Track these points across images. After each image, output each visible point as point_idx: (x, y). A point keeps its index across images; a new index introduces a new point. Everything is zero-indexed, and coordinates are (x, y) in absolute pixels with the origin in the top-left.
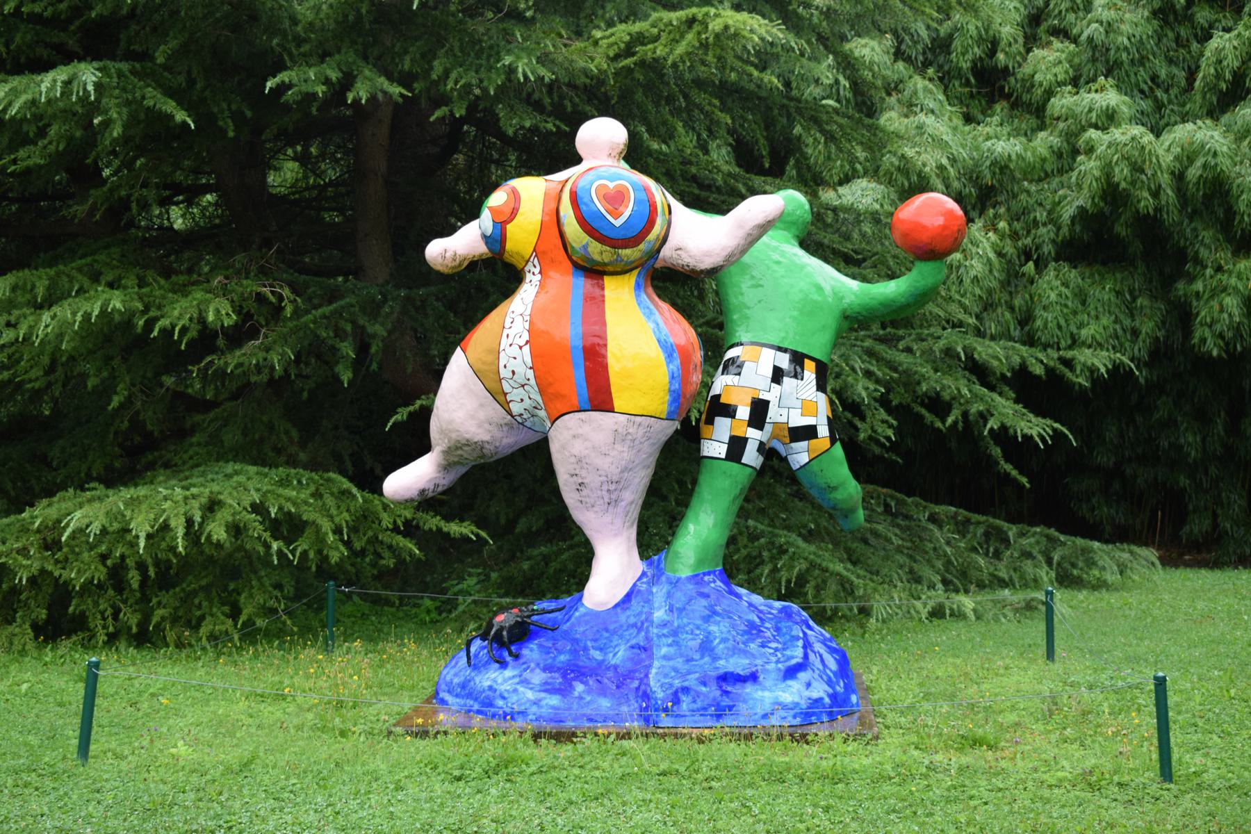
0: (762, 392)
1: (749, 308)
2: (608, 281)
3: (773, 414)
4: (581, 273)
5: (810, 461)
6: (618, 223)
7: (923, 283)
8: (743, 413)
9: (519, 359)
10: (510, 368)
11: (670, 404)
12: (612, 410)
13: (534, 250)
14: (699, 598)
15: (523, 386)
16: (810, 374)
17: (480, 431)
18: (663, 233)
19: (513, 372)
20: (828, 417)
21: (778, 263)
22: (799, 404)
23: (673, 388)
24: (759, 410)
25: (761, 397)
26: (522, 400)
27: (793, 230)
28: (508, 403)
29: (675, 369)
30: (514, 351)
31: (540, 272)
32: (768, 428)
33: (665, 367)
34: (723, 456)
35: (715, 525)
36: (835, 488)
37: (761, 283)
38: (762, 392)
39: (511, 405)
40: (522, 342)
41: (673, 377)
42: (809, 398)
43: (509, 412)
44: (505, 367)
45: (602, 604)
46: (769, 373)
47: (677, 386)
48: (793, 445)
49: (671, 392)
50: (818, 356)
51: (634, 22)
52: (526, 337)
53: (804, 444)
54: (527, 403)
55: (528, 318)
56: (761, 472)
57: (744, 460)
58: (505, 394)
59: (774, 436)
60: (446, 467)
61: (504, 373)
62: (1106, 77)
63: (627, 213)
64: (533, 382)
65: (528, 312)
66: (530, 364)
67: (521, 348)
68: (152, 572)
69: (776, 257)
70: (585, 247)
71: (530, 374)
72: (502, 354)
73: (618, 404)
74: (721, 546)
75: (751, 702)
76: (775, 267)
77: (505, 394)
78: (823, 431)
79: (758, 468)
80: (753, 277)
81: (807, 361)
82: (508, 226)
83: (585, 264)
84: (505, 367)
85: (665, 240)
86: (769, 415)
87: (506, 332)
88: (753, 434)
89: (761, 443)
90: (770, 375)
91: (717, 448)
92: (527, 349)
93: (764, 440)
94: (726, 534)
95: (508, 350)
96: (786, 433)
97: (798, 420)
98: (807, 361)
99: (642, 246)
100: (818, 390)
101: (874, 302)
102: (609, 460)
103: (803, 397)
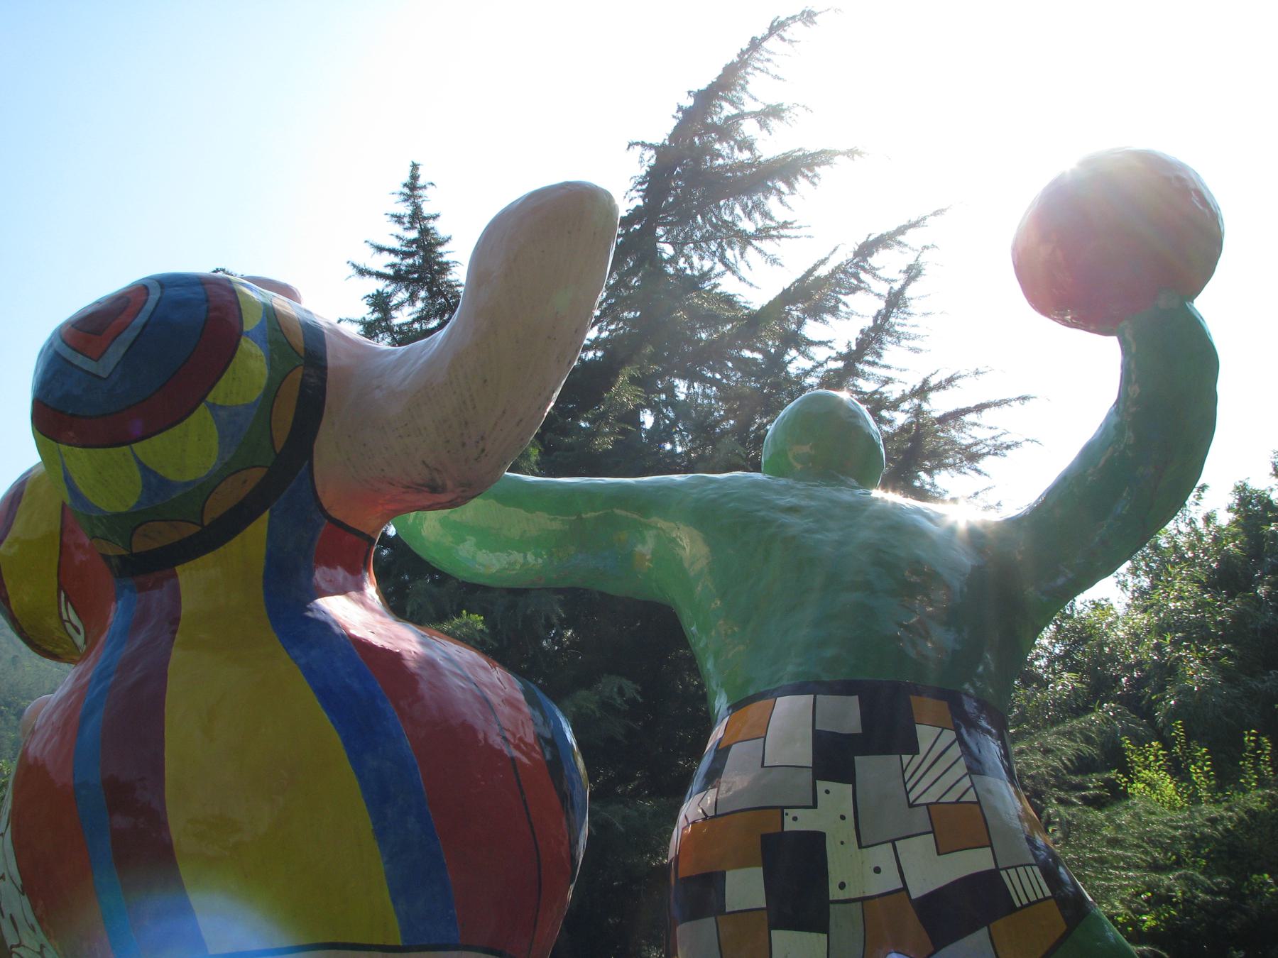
22: (920, 819)
25: (789, 826)
42: (951, 797)
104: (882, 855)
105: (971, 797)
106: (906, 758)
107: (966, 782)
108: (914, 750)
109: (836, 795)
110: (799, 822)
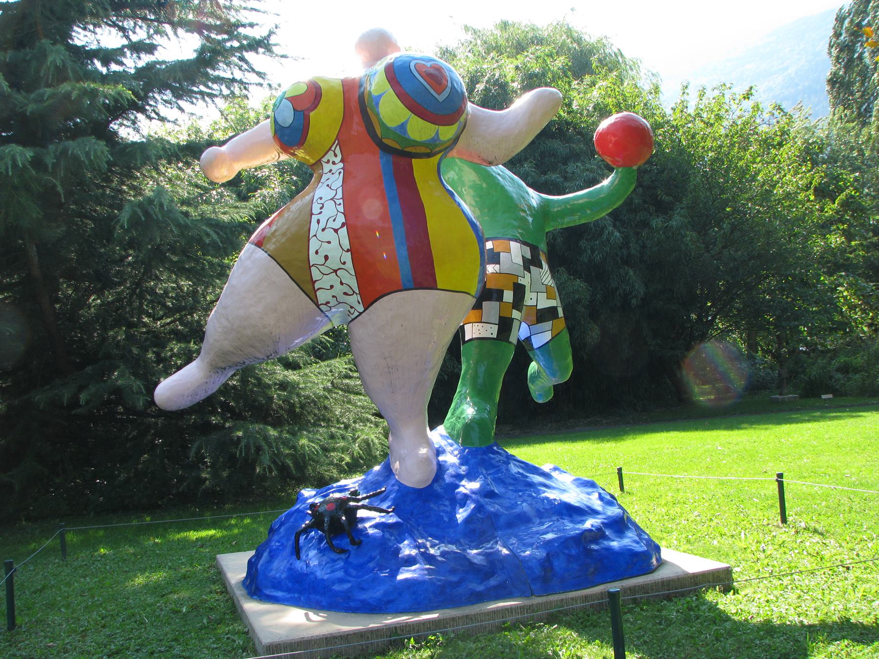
2: (414, 161)
5: (553, 338)
6: (441, 98)
8: (508, 296)
9: (335, 243)
10: (322, 254)
12: (431, 285)
13: (337, 138)
14: (625, 490)
15: (335, 271)
19: (326, 258)
22: (544, 288)
24: (519, 291)
26: (332, 287)
28: (315, 292)
30: (329, 235)
31: (342, 161)
34: (495, 336)
38: (520, 278)
39: (318, 293)
40: (337, 225)
43: (315, 301)
44: (317, 252)
52: (341, 219)
54: (339, 289)
55: (341, 201)
58: (314, 282)
60: (216, 368)
61: (313, 259)
62: (279, 193)
64: (349, 265)
65: (340, 195)
67: (336, 231)
68: (537, 479)
70: (403, 126)
71: (347, 257)
72: (313, 242)
77: (314, 282)
83: (398, 147)
84: (317, 252)
87: (314, 218)
95: (320, 235)
97: (544, 303)
110: (521, 281)
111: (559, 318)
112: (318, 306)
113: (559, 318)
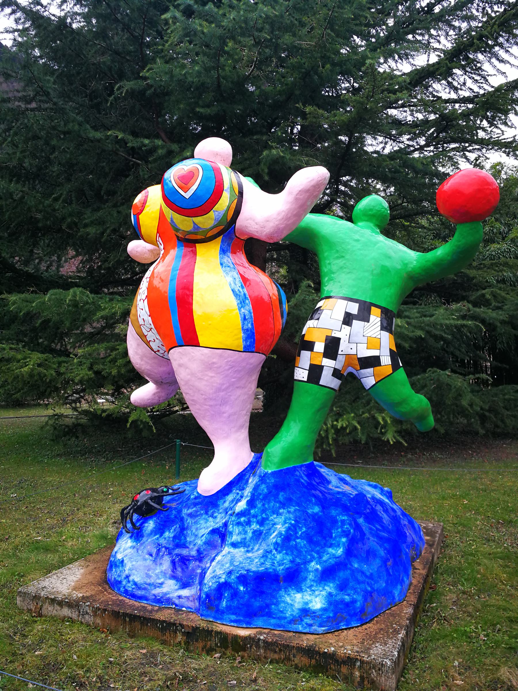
0: (334, 332)
1: (333, 273)
3: (344, 348)
4: (182, 244)
5: (376, 383)
6: (187, 195)
7: (463, 241)
8: (320, 347)
11: (246, 340)
12: (197, 345)
13: (158, 232)
16: (375, 318)
17: (143, 363)
18: (234, 205)
20: (390, 350)
21: (357, 241)
22: (365, 340)
23: (245, 327)
25: (333, 335)
27: (374, 221)
29: (247, 313)
32: (341, 358)
33: (238, 311)
35: (301, 431)
36: (399, 404)
37: (343, 255)
41: (245, 319)
42: (374, 336)
45: (206, 491)
46: (341, 317)
47: (250, 326)
48: (363, 371)
49: (245, 331)
50: (383, 305)
51: (473, 278)
53: (370, 370)
56: (340, 393)
57: (321, 382)
59: (348, 363)
63: (194, 188)
66: (149, 314)
69: (357, 237)
73: (202, 340)
74: (308, 447)
75: (282, 605)
76: (355, 243)
78: (386, 360)
79: (337, 388)
80: (337, 251)
81: (373, 308)
82: (140, 216)
85: (237, 212)
86: (341, 348)
88: (328, 363)
89: (335, 369)
90: (342, 319)
91: (301, 373)
92: (146, 301)
93: (339, 367)
94: (315, 437)
96: (357, 362)
97: (365, 352)
98: (373, 308)
99: (212, 214)
100: (381, 329)
101: (429, 264)
102: (204, 383)
103: (368, 335)
104: (354, 346)
105: (379, 337)
106: (366, 323)
107: (379, 332)
108: (368, 322)
109: (346, 328)
111: (381, 365)
112: (155, 352)
113: (381, 365)
